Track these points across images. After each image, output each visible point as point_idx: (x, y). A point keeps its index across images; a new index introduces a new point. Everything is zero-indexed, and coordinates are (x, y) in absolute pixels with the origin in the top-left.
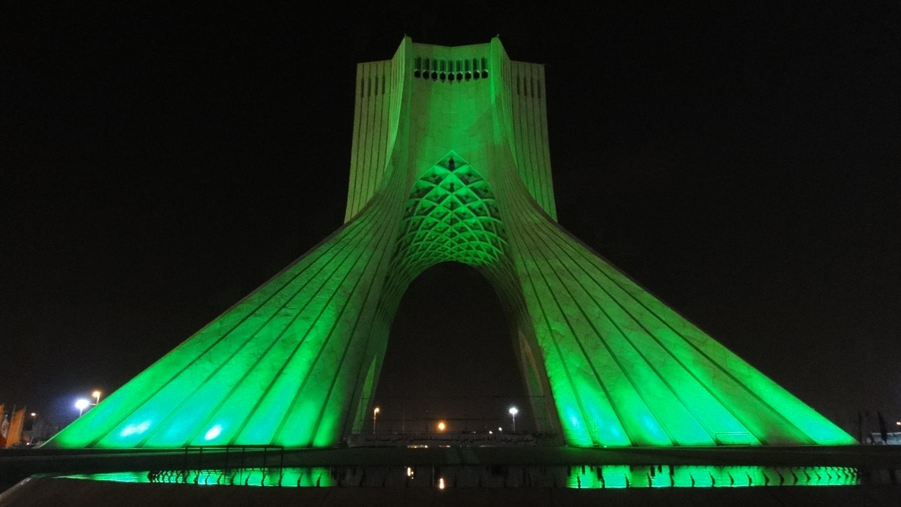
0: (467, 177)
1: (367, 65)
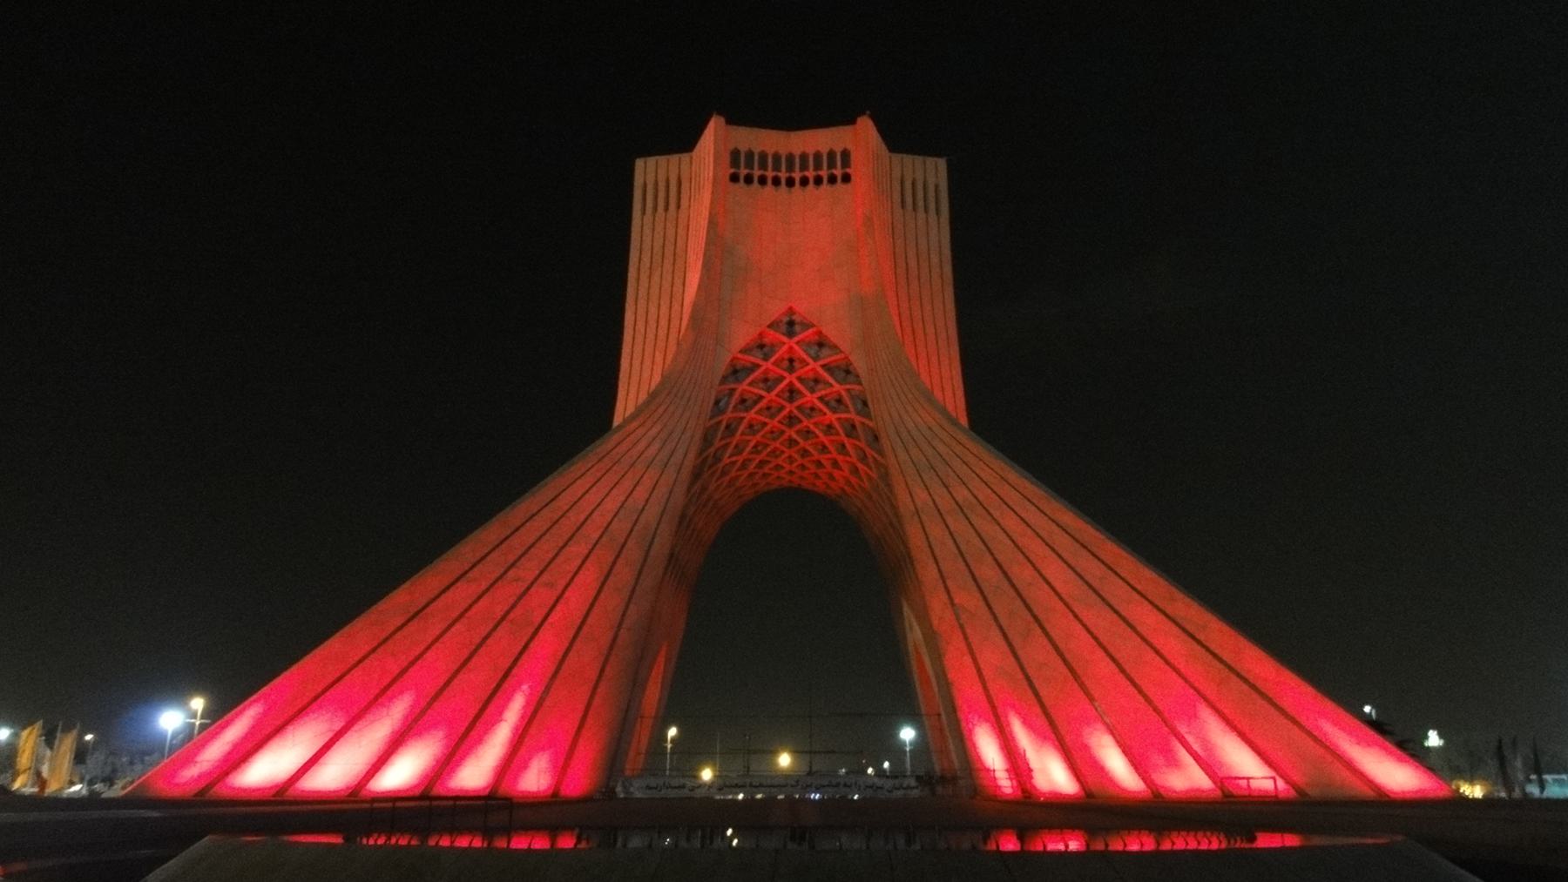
1: (651, 161)
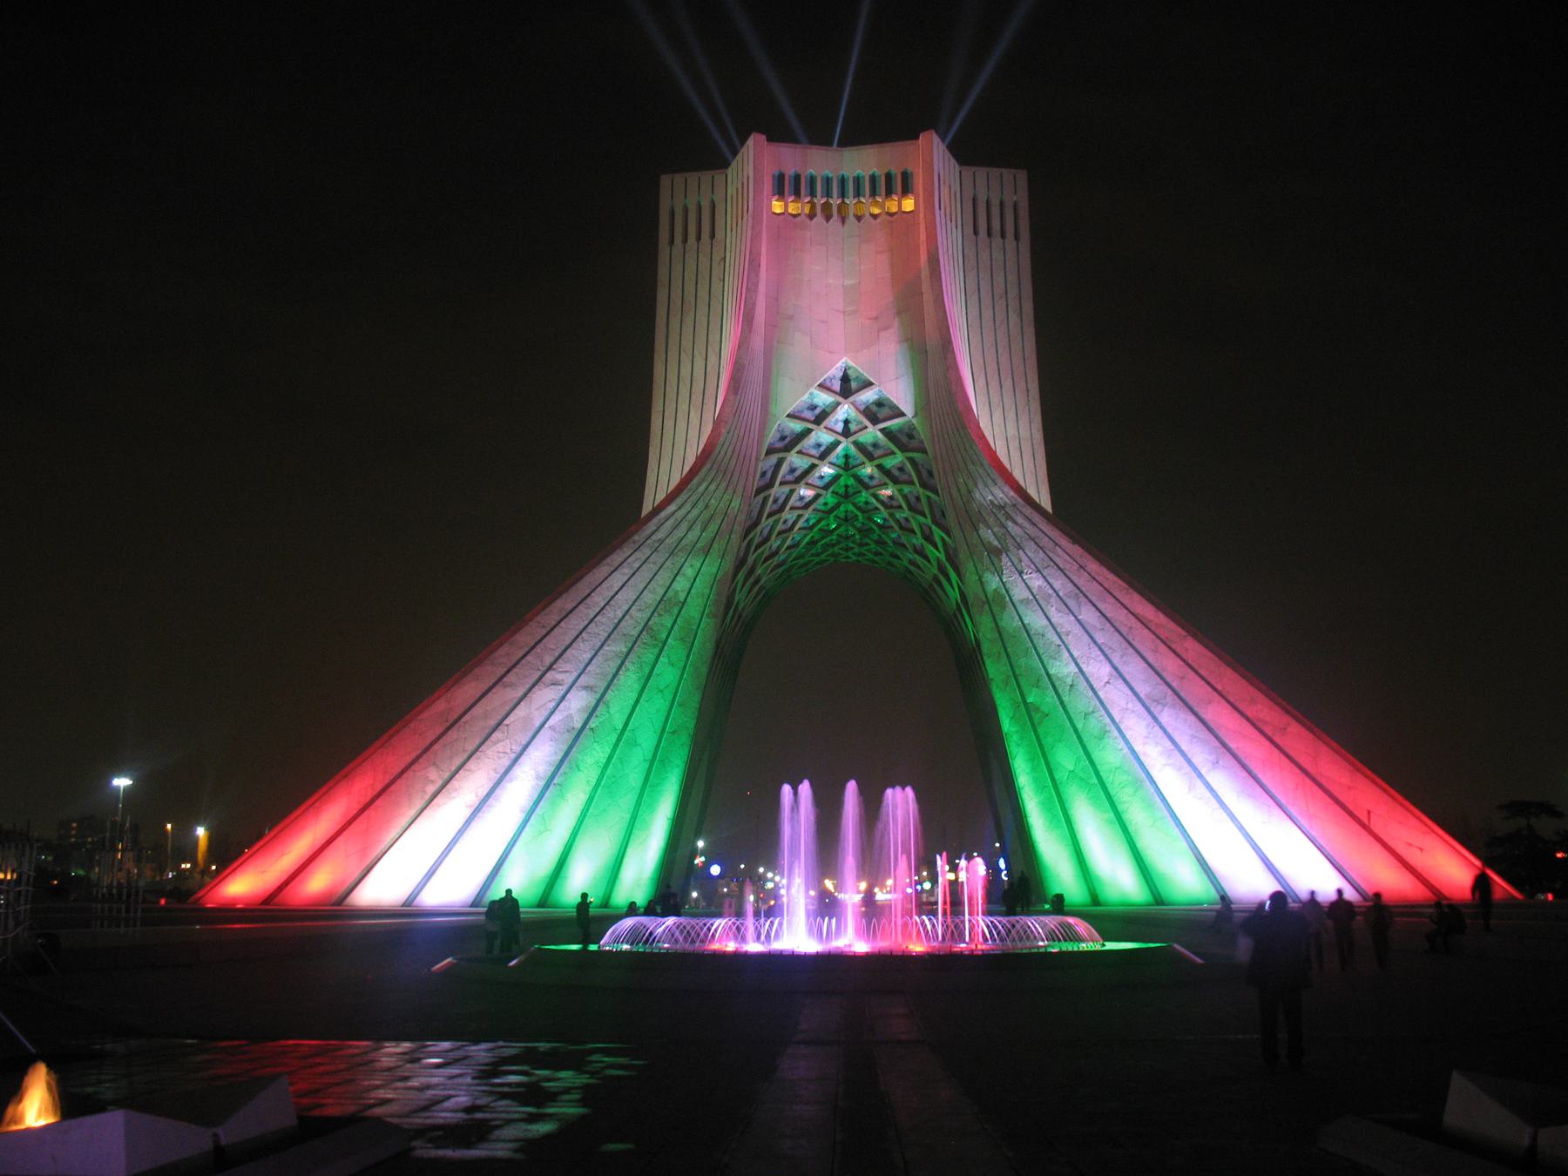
0: (874, 408)
1: (679, 178)
